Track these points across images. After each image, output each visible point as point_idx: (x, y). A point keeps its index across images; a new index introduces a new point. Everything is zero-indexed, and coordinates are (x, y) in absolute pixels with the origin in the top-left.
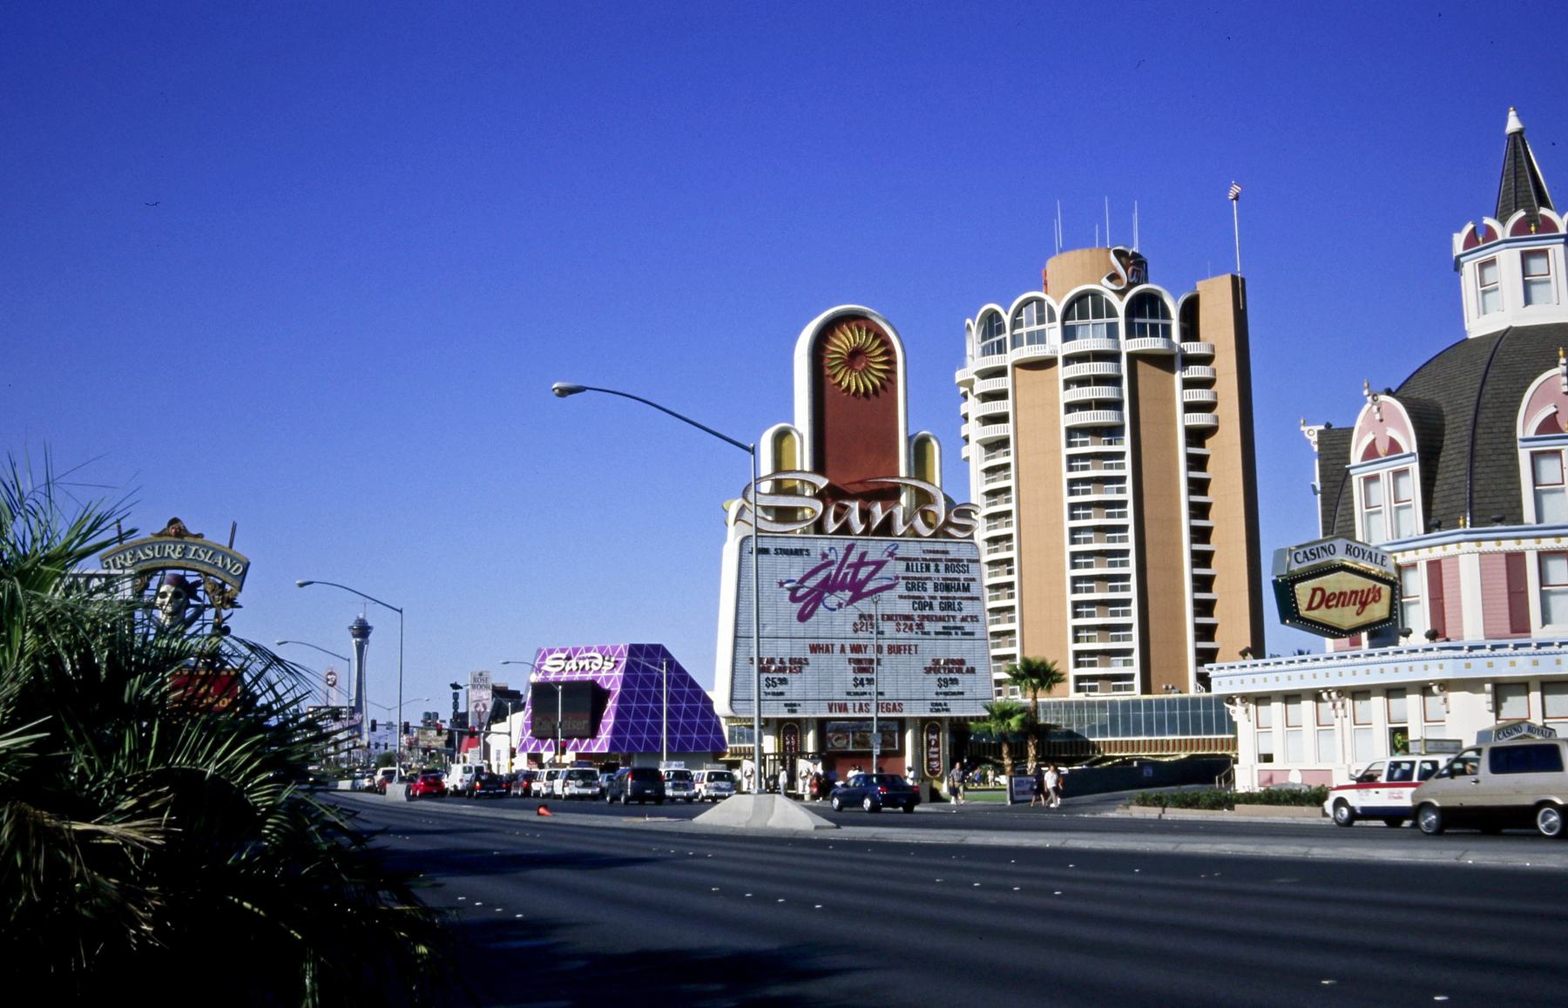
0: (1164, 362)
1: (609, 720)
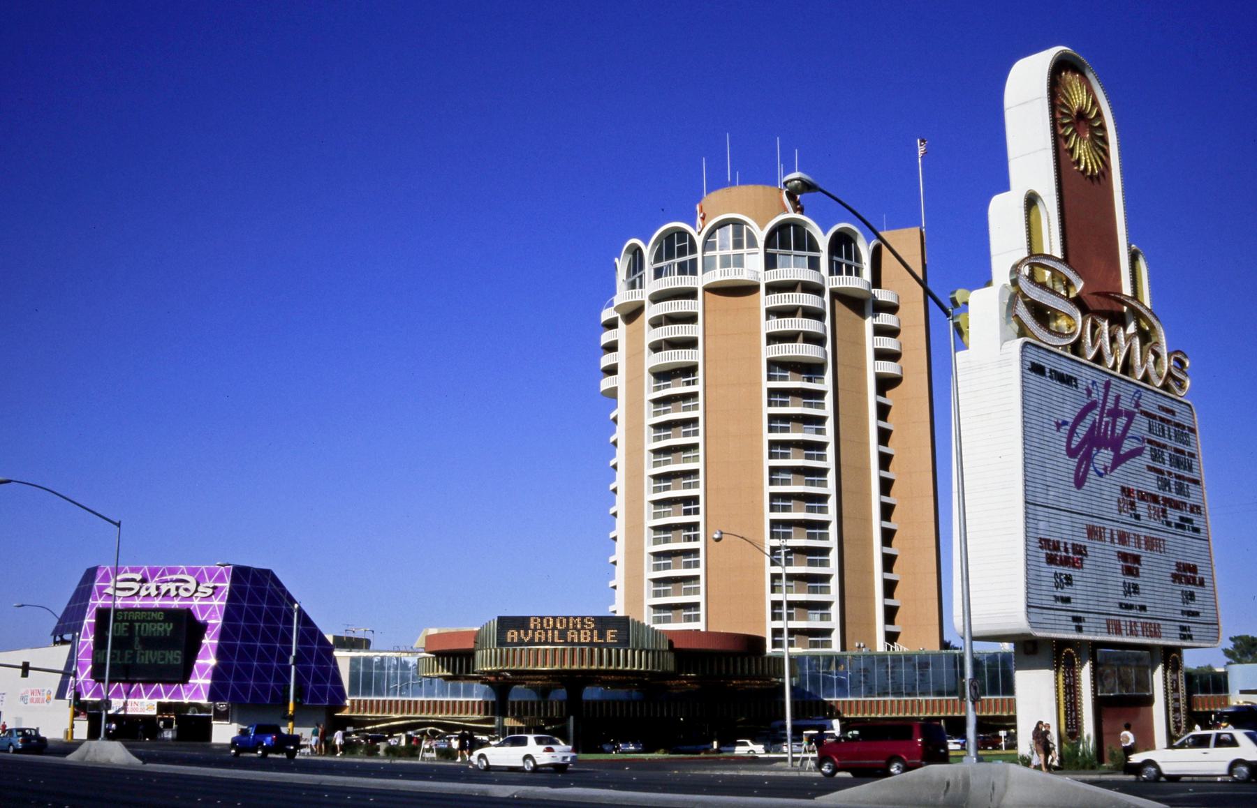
0: (857, 304)
1: (207, 660)
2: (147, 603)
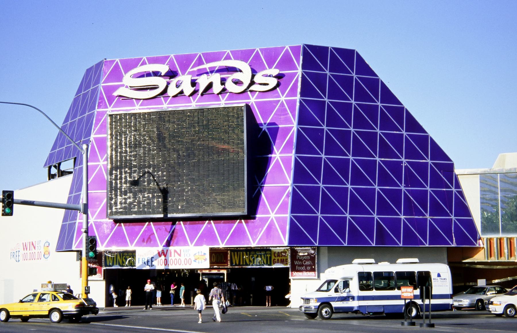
2: (181, 106)
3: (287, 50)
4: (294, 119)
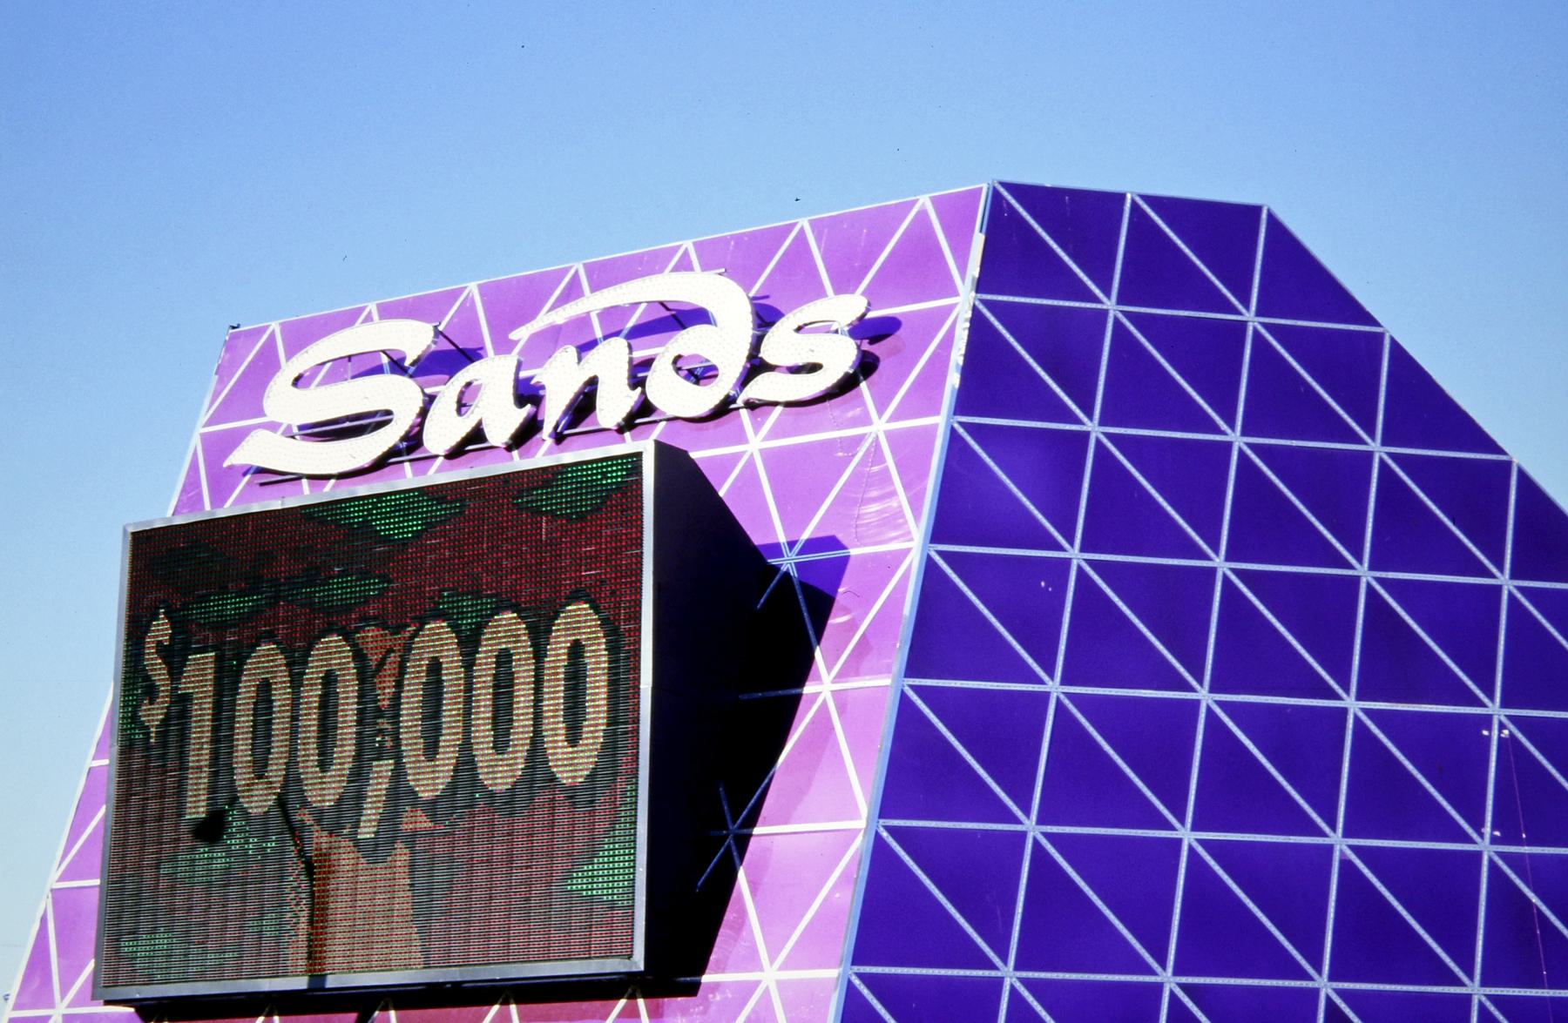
3: (922, 216)
4: (917, 516)
